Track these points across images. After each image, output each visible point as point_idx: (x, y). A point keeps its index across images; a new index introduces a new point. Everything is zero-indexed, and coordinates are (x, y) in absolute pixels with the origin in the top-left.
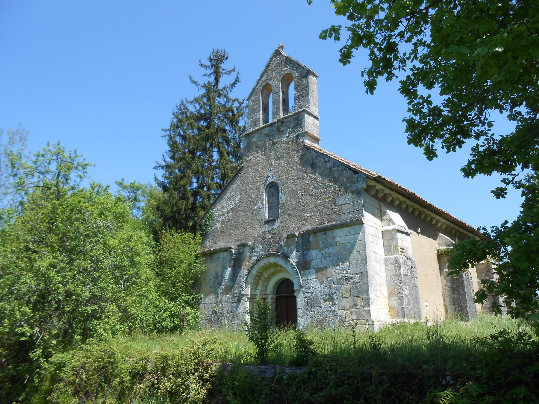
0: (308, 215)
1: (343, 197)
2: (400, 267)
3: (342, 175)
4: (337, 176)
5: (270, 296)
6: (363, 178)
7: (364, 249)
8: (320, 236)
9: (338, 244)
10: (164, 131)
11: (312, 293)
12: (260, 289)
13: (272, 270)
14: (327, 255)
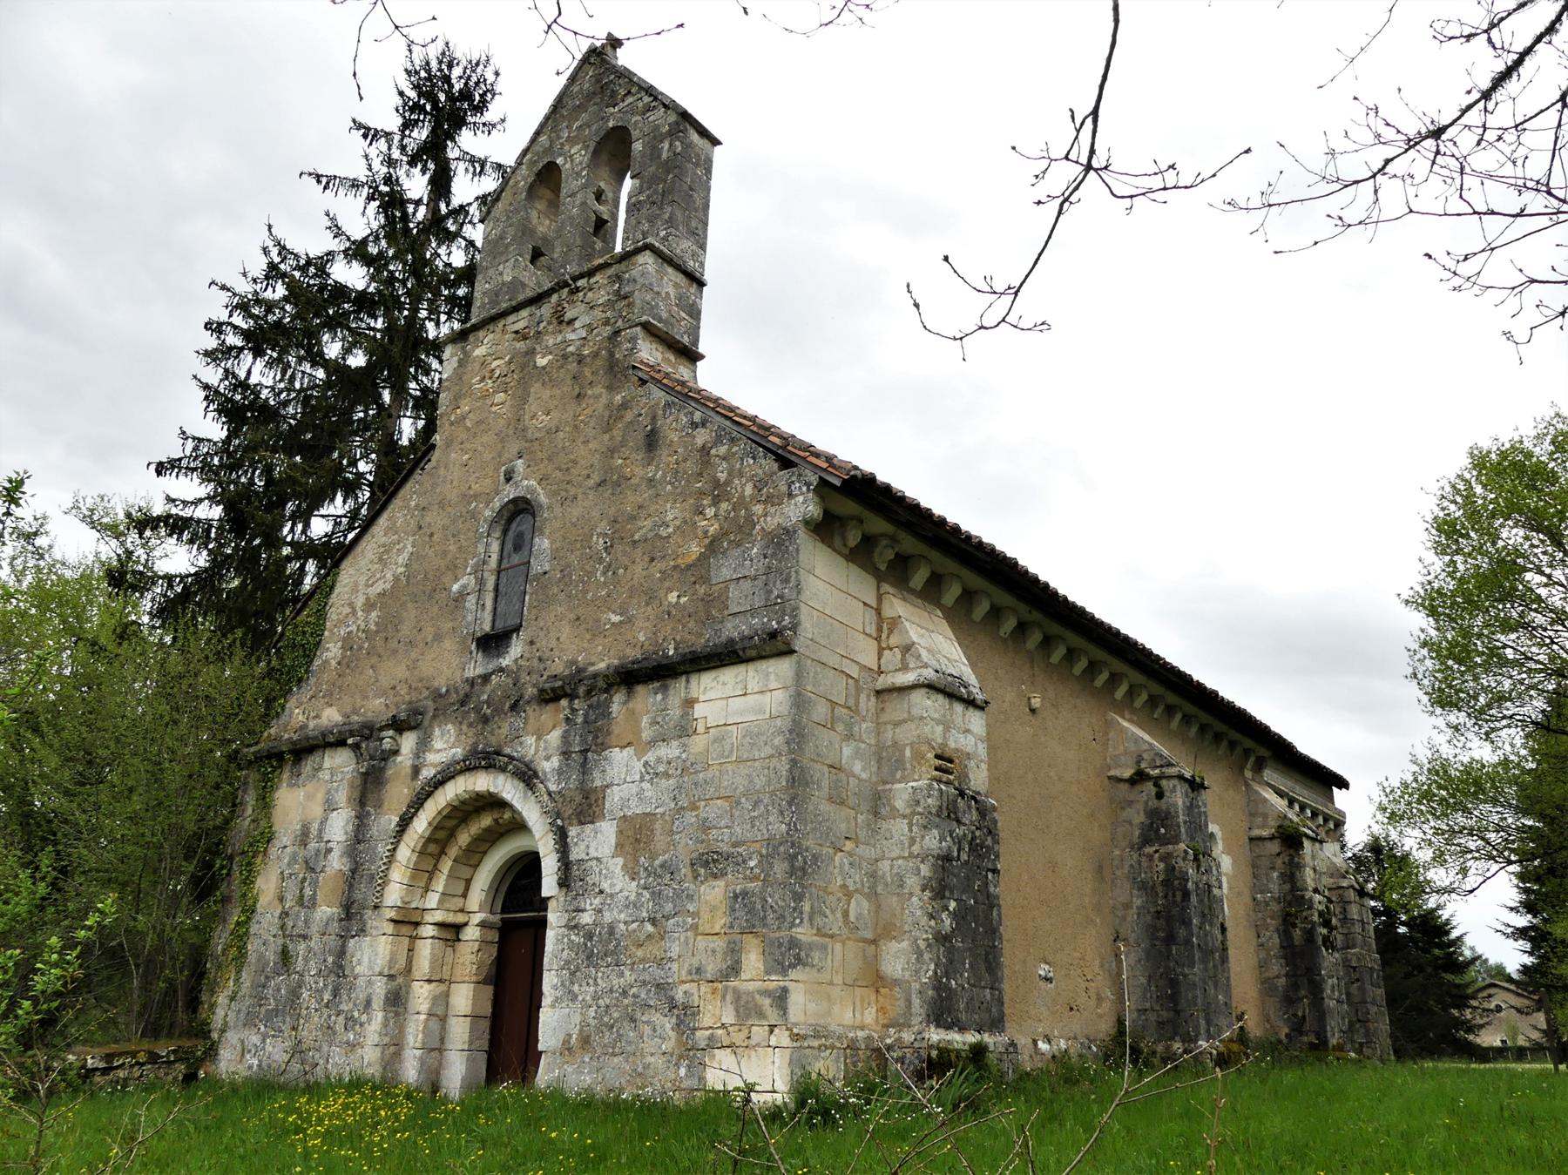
1: (737, 552)
3: (741, 475)
4: (722, 476)
5: (477, 918)
6: (808, 484)
8: (647, 699)
9: (701, 729)
12: (440, 889)
13: (486, 821)
14: (661, 769)
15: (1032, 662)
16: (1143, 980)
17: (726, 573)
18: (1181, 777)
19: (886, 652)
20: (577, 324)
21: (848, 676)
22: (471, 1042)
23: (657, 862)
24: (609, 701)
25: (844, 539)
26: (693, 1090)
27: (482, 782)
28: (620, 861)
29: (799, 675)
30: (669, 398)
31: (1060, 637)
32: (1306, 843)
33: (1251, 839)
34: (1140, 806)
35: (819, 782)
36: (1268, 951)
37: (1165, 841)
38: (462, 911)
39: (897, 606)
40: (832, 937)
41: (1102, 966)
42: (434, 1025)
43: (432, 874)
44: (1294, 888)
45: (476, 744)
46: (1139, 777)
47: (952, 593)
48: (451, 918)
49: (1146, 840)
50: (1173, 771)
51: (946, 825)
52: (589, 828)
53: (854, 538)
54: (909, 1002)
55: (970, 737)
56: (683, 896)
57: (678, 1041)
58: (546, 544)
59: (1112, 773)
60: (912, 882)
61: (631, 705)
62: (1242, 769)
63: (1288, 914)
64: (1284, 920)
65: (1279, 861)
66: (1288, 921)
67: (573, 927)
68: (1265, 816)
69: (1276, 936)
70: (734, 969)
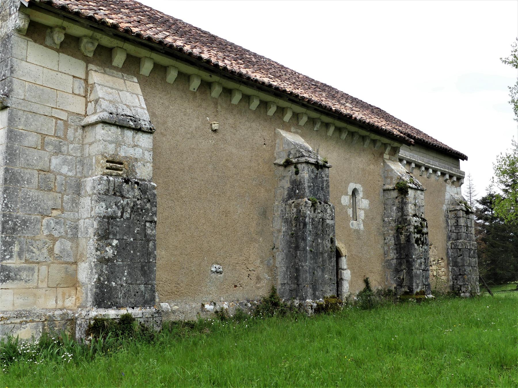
6: (16, 7)
15: (216, 104)
16: (284, 269)
18: (307, 163)
19: (89, 104)
26: (115, 319)
29: (11, 120)
31: (238, 90)
32: (410, 191)
33: (384, 190)
34: (288, 179)
35: (29, 182)
36: (389, 246)
37: (299, 197)
39: (96, 77)
40: (38, 263)
41: (262, 262)
44: (403, 215)
46: (288, 163)
49: (290, 197)
50: (303, 159)
51: (113, 199)
53: (59, 38)
54: (87, 294)
55: (137, 149)
59: (276, 162)
60: (91, 231)
62: (382, 154)
63: (398, 228)
64: (397, 231)
65: (397, 201)
66: (398, 231)
68: (391, 178)
69: (393, 239)
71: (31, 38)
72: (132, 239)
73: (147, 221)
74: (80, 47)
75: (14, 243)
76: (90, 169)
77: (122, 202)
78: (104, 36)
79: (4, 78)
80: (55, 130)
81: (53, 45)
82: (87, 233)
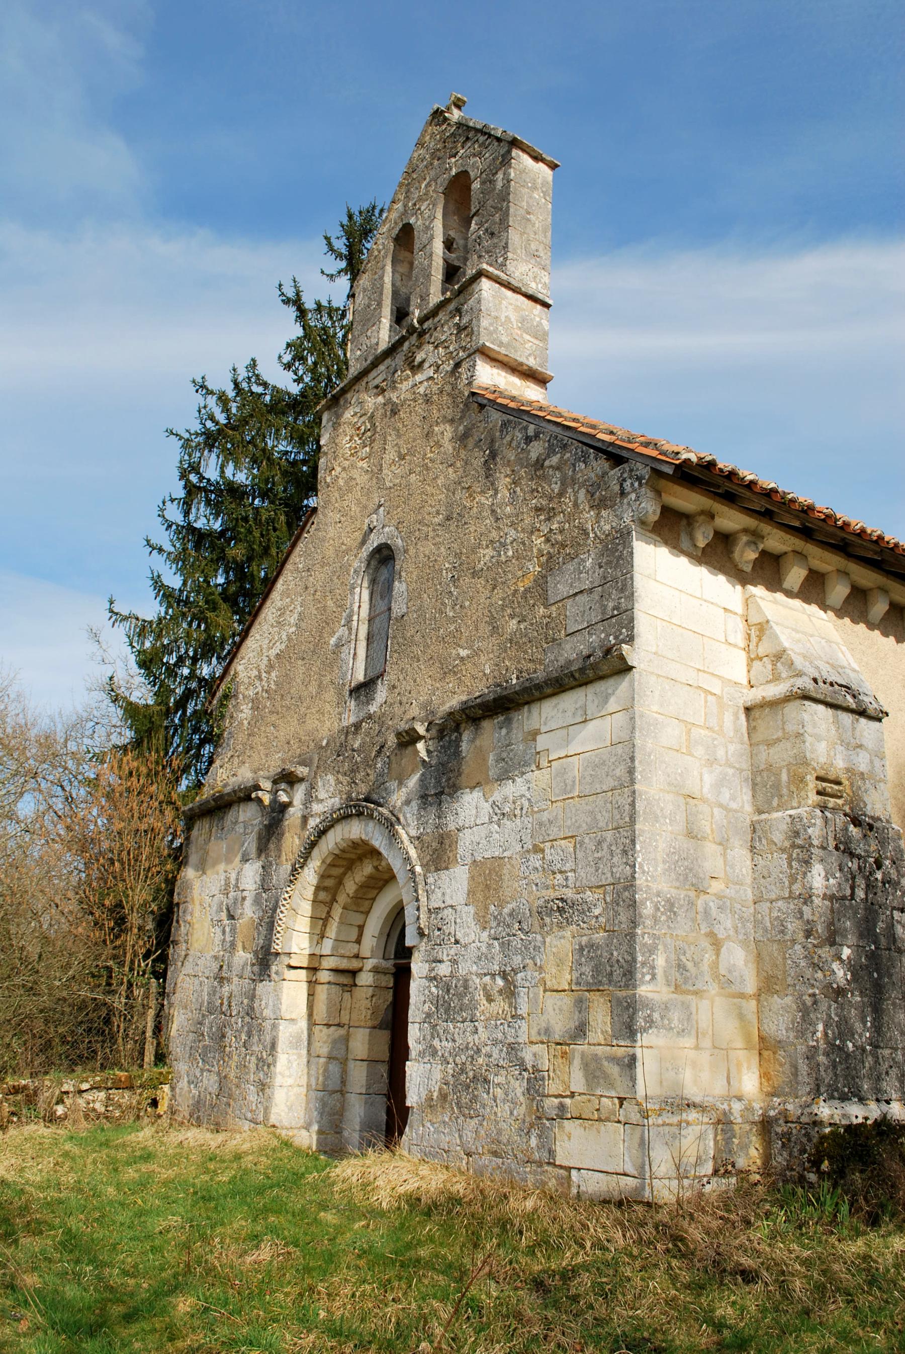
0: (464, 653)
1: (571, 567)
2: (807, 863)
3: (574, 481)
5: (369, 964)
6: (639, 479)
7: (626, 778)
8: (491, 732)
10: (804, 552)
11: (454, 962)
17: (563, 590)
19: (757, 663)
20: (426, 365)
21: (707, 692)
22: (368, 1087)
23: (506, 911)
24: (458, 740)
25: (692, 538)
27: (355, 830)
28: (471, 909)
30: (506, 417)
38: (357, 956)
42: (334, 1068)
43: (325, 921)
45: (349, 794)
47: (839, 591)
48: (344, 964)
52: (444, 874)
56: (531, 950)
57: (529, 1107)
58: (403, 587)
61: (478, 743)
67: (433, 979)
70: (581, 1030)
71: (659, 535)
72: (873, 947)
73: (894, 908)
74: (732, 552)
75: (656, 948)
76: (773, 797)
77: (850, 864)
78: (775, 530)
79: (616, 612)
80: (706, 715)
81: (691, 549)
82: (782, 932)
